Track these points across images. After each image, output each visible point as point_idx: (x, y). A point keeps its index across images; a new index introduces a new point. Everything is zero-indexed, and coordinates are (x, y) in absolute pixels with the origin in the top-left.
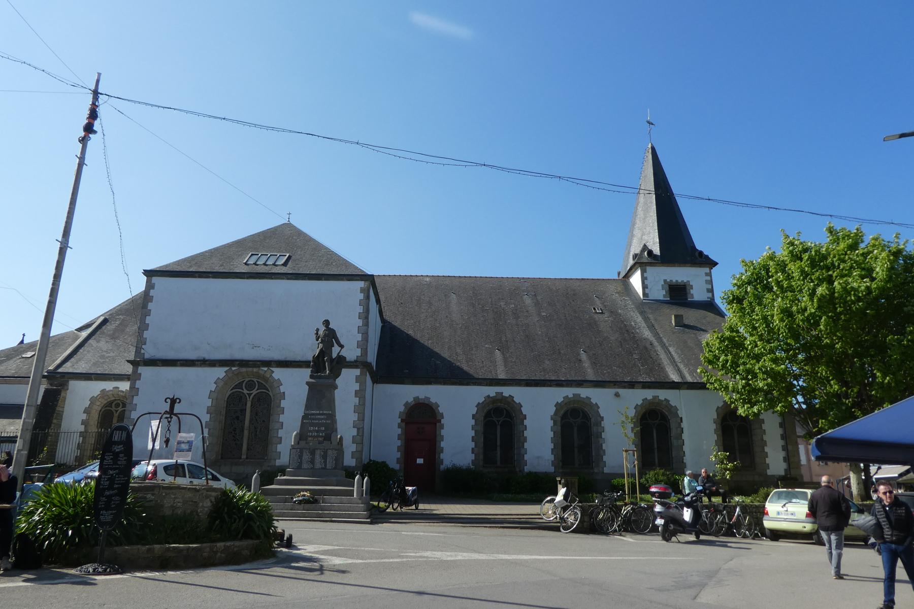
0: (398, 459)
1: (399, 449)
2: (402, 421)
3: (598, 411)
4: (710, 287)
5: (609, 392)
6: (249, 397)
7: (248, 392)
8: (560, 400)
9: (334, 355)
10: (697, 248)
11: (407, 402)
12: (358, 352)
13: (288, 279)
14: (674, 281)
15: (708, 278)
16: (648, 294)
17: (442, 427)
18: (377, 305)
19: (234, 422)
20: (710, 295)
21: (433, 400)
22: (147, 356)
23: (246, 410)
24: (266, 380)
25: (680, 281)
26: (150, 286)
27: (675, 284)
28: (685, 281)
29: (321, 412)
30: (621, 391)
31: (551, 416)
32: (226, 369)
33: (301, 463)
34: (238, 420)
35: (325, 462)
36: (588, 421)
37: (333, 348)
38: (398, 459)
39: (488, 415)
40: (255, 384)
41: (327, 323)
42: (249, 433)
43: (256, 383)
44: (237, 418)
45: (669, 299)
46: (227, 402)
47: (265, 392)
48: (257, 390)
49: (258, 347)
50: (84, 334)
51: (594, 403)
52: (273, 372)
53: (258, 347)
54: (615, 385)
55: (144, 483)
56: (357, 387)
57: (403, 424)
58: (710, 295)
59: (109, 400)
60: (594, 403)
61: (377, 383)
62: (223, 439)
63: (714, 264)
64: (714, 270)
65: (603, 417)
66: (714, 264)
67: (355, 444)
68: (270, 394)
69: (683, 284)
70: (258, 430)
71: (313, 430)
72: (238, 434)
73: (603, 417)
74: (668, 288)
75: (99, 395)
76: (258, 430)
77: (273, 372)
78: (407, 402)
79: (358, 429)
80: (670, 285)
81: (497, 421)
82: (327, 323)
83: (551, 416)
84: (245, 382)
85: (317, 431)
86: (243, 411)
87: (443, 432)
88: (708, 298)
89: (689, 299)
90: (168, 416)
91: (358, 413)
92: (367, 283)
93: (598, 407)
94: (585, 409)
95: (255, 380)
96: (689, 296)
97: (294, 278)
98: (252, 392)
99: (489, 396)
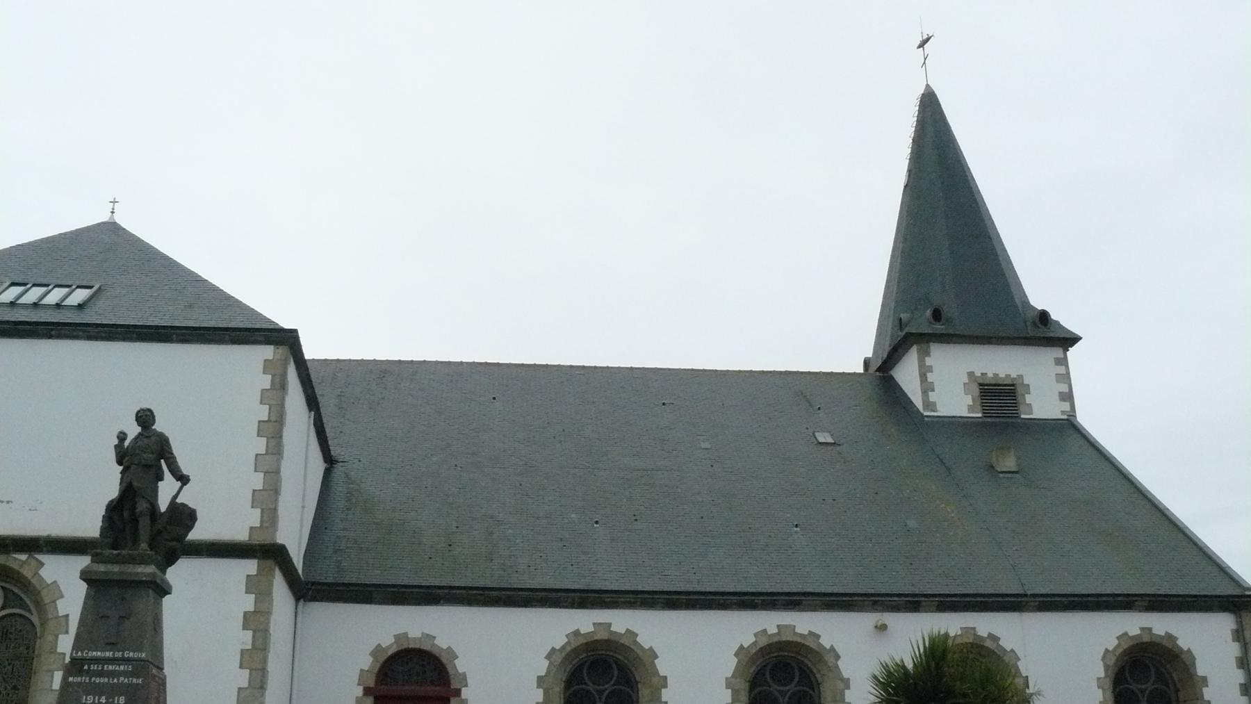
3: (837, 667)
4: (1066, 390)
5: (863, 621)
8: (748, 640)
9: (163, 504)
10: (1032, 303)
11: (379, 645)
12: (254, 518)
13: (90, 338)
14: (990, 375)
15: (1061, 370)
18: (310, 411)
20: (1066, 406)
21: (442, 642)
24: (25, 585)
25: (1002, 375)
27: (993, 382)
28: (1014, 375)
29: (119, 655)
30: (891, 619)
31: (727, 678)
37: (160, 483)
41: (145, 418)
45: (980, 415)
47: (21, 616)
49: (8, 502)
52: (42, 564)
53: (8, 502)
56: (249, 603)
58: (1066, 406)
60: (828, 647)
63: (1070, 340)
64: (1073, 352)
66: (1070, 340)
68: (35, 619)
69: (1010, 383)
74: (976, 391)
77: (42, 564)
78: (379, 645)
80: (981, 385)
82: (145, 418)
83: (727, 678)
88: (1063, 412)
89: (1023, 416)
92: (283, 351)
93: (838, 657)
94: (806, 661)
96: (1022, 408)
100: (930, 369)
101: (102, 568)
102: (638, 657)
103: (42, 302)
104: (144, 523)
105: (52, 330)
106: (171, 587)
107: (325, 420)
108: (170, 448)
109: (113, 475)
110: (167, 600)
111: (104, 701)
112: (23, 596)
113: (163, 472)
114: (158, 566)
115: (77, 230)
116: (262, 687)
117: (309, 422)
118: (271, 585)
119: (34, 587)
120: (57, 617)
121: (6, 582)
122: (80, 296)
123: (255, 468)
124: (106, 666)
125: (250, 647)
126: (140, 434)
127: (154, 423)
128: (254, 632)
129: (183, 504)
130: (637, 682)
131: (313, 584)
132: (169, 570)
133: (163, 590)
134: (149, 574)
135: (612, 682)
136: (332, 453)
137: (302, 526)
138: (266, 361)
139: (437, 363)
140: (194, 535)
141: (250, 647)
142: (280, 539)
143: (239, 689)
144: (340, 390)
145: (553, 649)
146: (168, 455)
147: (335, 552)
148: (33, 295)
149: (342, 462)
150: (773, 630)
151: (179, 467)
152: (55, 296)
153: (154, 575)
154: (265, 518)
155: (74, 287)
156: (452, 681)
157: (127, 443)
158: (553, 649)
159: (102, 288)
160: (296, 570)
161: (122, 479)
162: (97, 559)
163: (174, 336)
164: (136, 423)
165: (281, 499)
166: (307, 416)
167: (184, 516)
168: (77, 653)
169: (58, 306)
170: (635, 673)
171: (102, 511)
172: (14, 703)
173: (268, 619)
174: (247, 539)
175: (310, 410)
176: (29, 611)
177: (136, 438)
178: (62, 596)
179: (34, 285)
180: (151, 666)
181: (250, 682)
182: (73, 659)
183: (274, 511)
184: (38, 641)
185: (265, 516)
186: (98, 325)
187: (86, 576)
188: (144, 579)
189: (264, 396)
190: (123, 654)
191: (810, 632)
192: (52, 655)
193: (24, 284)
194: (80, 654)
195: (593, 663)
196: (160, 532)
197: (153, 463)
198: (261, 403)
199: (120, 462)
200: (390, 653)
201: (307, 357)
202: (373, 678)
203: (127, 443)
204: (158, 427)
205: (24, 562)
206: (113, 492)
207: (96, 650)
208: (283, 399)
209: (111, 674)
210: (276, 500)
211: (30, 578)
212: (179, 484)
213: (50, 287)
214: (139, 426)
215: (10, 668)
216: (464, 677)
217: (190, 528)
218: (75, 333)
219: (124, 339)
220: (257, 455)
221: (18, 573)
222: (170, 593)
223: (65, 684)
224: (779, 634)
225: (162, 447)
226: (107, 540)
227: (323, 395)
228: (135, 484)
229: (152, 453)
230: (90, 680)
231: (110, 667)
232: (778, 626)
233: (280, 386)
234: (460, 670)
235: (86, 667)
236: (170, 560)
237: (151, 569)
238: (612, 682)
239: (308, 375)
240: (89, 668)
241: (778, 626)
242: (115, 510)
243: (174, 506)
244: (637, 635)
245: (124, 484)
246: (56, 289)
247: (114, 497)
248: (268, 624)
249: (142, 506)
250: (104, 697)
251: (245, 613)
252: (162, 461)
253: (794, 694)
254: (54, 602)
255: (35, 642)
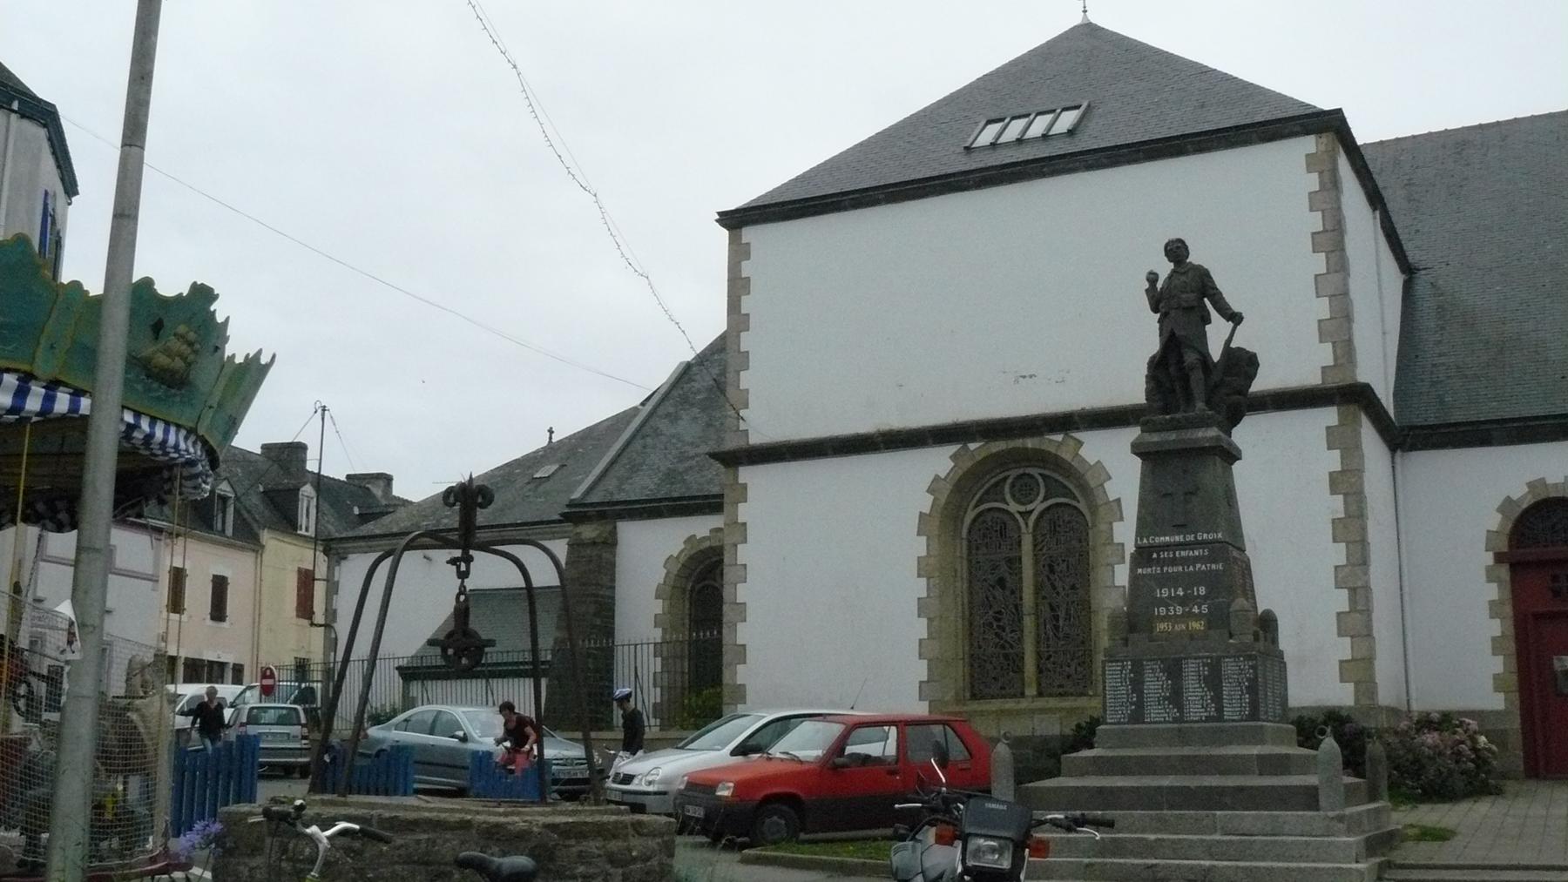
0: (1496, 677)
1: (1497, 645)
2: (1499, 558)
6: (1027, 524)
7: (1022, 509)
9: (1216, 352)
12: (1325, 354)
19: (994, 598)
22: (755, 439)
23: (1020, 559)
26: (738, 253)
29: (1190, 538)
32: (953, 449)
33: (1140, 705)
34: (1003, 587)
35: (1218, 699)
37: (1208, 327)
40: (1037, 481)
41: (1177, 251)
42: (1038, 625)
43: (1040, 480)
44: (1001, 582)
46: (969, 542)
48: (1046, 499)
49: (1031, 376)
50: (649, 407)
52: (1080, 443)
53: (1031, 376)
55: (345, 804)
56: (1333, 461)
57: (1504, 572)
59: (707, 562)
61: (1404, 451)
62: (972, 645)
68: (1082, 506)
70: (1062, 614)
71: (1170, 597)
72: (1008, 630)
75: (682, 551)
76: (1062, 614)
79: (1353, 591)
82: (1177, 251)
84: (1009, 481)
85: (1183, 601)
86: (1014, 562)
90: (458, 553)
92: (1327, 138)
95: (1034, 471)
98: (1030, 507)
101: (1155, 438)
103: (1026, 137)
104: (1197, 377)
105: (1043, 167)
106: (1239, 451)
107: (1394, 219)
108: (1213, 282)
109: (1151, 323)
110: (1237, 467)
111: (1182, 594)
112: (1066, 483)
113: (1209, 313)
114: (1221, 428)
115: (1048, 42)
116: (1364, 562)
117: (1375, 225)
118: (1357, 435)
119: (1076, 469)
120: (1108, 502)
121: (1045, 468)
122: (1067, 120)
123: (1317, 293)
124: (1177, 553)
125: (1343, 516)
126: (1174, 271)
127: (1188, 254)
128: (1346, 495)
129: (1239, 349)
131: (1412, 428)
132: (1235, 431)
133: (1231, 455)
134: (1212, 438)
136: (1410, 259)
137: (1385, 361)
138: (1307, 155)
139: (1533, 118)
140: (1259, 385)
141: (1343, 516)
142: (1363, 376)
143: (1336, 567)
144: (1408, 177)
146: (1212, 292)
147: (1433, 384)
148: (1014, 129)
149: (1425, 269)
151: (1226, 303)
152: (1039, 126)
153: (1218, 438)
154: (1339, 351)
155: (1058, 111)
157: (1159, 285)
159: (1093, 105)
160: (1386, 412)
161: (1161, 329)
162: (1148, 428)
163: (1189, 146)
164: (1166, 259)
165: (1355, 326)
166: (1371, 221)
167: (1242, 363)
168: (1141, 540)
169: (1045, 137)
171: (1144, 370)
172: (468, 880)
173: (1361, 478)
174: (1320, 382)
175: (1374, 210)
176: (1075, 498)
177: (1170, 277)
178: (1110, 478)
179: (1014, 118)
180: (1231, 548)
181: (1348, 558)
182: (1139, 548)
183: (1349, 342)
184: (1090, 532)
185: (1339, 351)
186: (1095, 150)
187: (1138, 449)
188: (1207, 445)
189: (1314, 201)
190: (1196, 537)
192: (1108, 547)
193: (1027, 115)
194: (1145, 541)
196: (1216, 386)
197: (1195, 304)
198: (1311, 210)
199: (1155, 309)
200: (1525, 506)
201: (1359, 142)
202: (1505, 543)
203: (1159, 285)
204: (1194, 258)
205: (1060, 444)
206: (1153, 345)
207: (1165, 535)
208: (1338, 200)
209: (1185, 561)
210: (1350, 329)
211: (1069, 460)
212: (1231, 324)
213: (1032, 117)
214: (1170, 261)
215: (1065, 565)
217: (1251, 377)
218: (1071, 165)
219: (1129, 162)
220: (1316, 276)
221: (1056, 456)
222: (1239, 459)
223: (1134, 579)
225: (1203, 282)
226: (1155, 405)
227: (1385, 188)
228: (1178, 333)
229: (1192, 292)
230: (1162, 570)
231: (1183, 553)
233: (1332, 184)
235: (1155, 556)
236: (1234, 419)
237: (1213, 432)
239: (1365, 166)
240: (1159, 555)
242: (1158, 367)
243: (1228, 352)
245: (1166, 335)
246: (1039, 117)
247: (1155, 352)
248: (1362, 484)
249: (1190, 358)
250: (1180, 589)
251: (1331, 474)
252: (1206, 299)
254: (1102, 485)
255: (1087, 534)
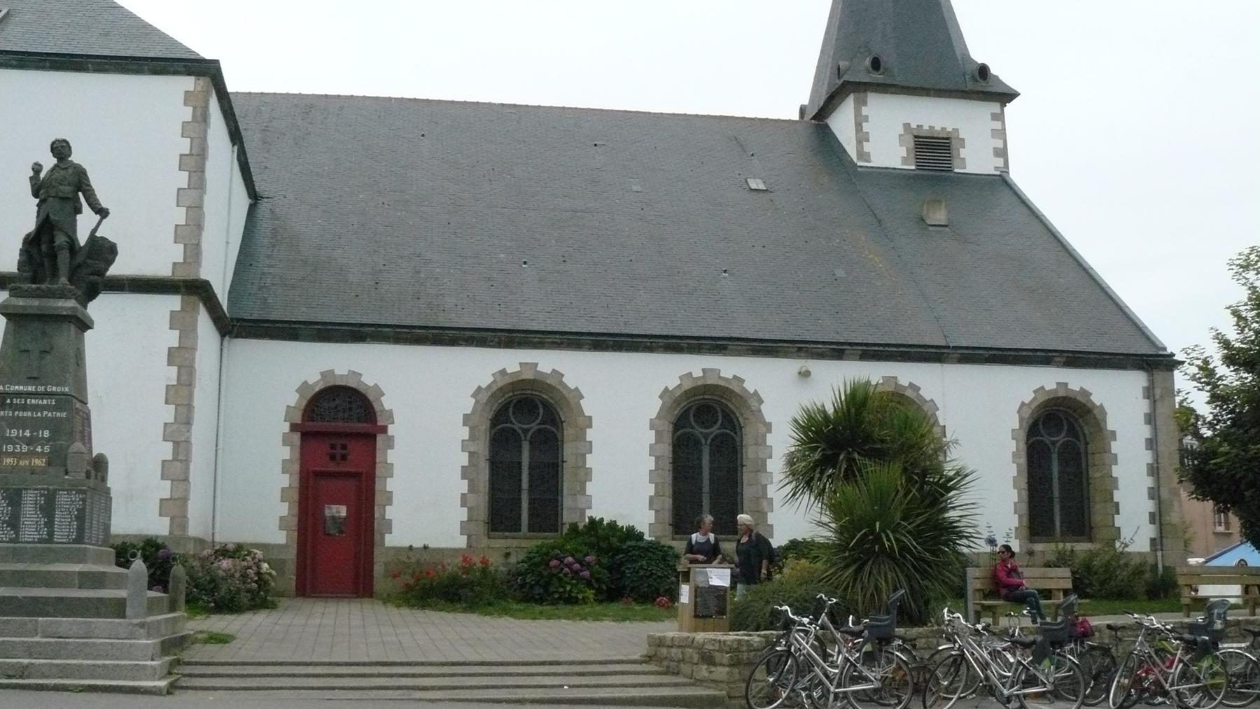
0: (282, 518)
2: (294, 427)
3: (760, 411)
5: (786, 368)
8: (673, 383)
9: (82, 237)
12: (177, 253)
14: (926, 127)
15: (998, 125)
16: (868, 154)
17: (390, 443)
20: (1000, 162)
25: (938, 128)
28: (949, 129)
29: (41, 389)
35: (50, 524)
36: (736, 433)
37: (78, 217)
38: (282, 518)
39: (499, 418)
41: (61, 149)
45: (913, 167)
51: (752, 391)
54: (800, 349)
56: (173, 338)
57: (297, 437)
58: (1000, 162)
60: (752, 391)
63: (1007, 96)
64: (1010, 108)
65: (770, 424)
66: (1007, 96)
67: (169, 482)
71: (17, 437)
73: (770, 424)
74: (912, 144)
79: (177, 444)
81: (523, 430)
82: (61, 149)
85: (30, 441)
87: (392, 456)
88: (996, 168)
89: (956, 170)
91: (177, 406)
92: (204, 82)
93: (761, 401)
96: (956, 162)
97: (14, 63)
99: (503, 372)
100: (866, 119)
102: (564, 397)
130: (562, 422)
135: (538, 421)
145: (479, 388)
150: (697, 373)
156: (379, 418)
158: (479, 388)
170: (561, 414)
191: (735, 377)
195: (519, 401)
200: (317, 389)
216: (390, 416)
224: (704, 377)
232: (703, 370)
234: (387, 407)
238: (538, 421)
241: (703, 370)
244: (563, 375)
253: (716, 437)
